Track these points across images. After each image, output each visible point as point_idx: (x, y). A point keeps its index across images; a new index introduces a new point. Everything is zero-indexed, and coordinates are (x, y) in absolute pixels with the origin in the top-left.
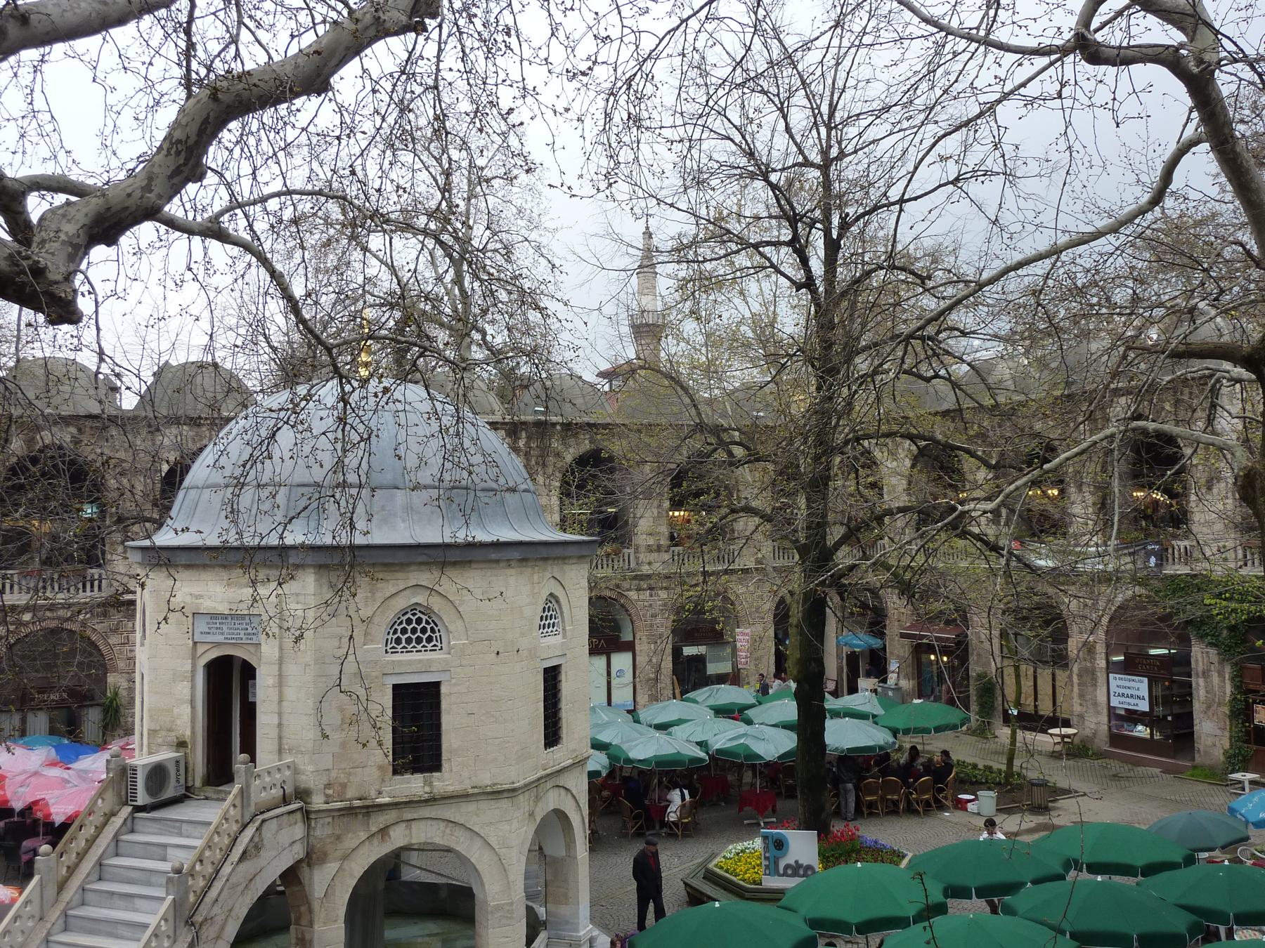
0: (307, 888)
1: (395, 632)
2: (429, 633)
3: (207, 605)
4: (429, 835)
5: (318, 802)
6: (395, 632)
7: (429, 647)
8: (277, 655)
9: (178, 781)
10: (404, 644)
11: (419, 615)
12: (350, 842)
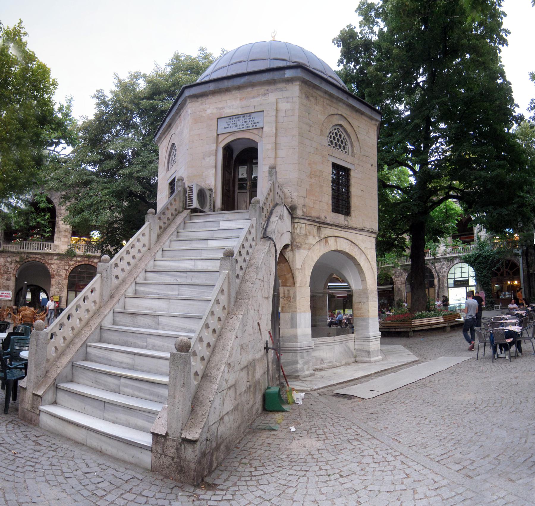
0: (291, 264)
3: (228, 112)
4: (344, 247)
5: (299, 213)
8: (274, 132)
9: (210, 205)
12: (312, 240)
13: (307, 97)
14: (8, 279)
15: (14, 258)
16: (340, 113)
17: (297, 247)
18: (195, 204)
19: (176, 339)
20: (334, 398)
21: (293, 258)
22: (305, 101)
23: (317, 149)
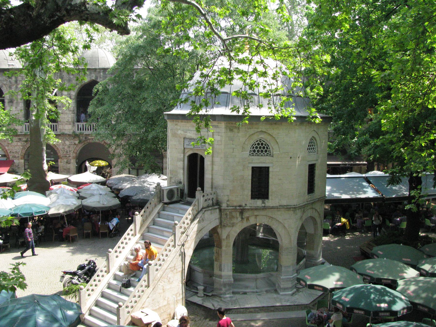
1: (253, 148)
2: (266, 149)
6: (253, 148)
7: (266, 154)
9: (178, 195)
10: (256, 152)
11: (262, 142)
13: (231, 130)
14: (68, 163)
15: (72, 141)
16: (260, 130)
17: (224, 226)
18: (166, 200)
19: (318, 172)
20: (153, 312)
21: (221, 232)
22: (229, 134)
23: (239, 162)
